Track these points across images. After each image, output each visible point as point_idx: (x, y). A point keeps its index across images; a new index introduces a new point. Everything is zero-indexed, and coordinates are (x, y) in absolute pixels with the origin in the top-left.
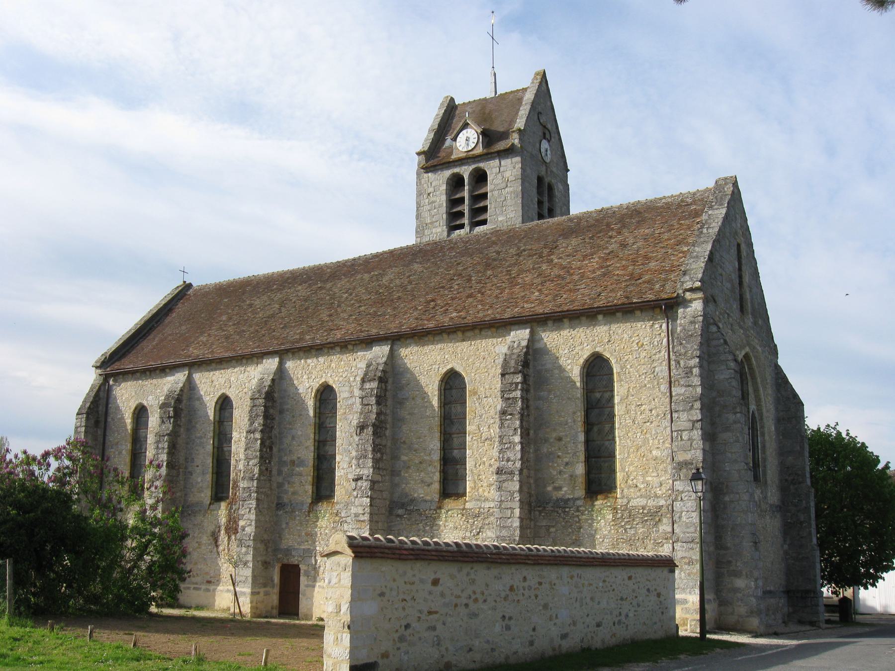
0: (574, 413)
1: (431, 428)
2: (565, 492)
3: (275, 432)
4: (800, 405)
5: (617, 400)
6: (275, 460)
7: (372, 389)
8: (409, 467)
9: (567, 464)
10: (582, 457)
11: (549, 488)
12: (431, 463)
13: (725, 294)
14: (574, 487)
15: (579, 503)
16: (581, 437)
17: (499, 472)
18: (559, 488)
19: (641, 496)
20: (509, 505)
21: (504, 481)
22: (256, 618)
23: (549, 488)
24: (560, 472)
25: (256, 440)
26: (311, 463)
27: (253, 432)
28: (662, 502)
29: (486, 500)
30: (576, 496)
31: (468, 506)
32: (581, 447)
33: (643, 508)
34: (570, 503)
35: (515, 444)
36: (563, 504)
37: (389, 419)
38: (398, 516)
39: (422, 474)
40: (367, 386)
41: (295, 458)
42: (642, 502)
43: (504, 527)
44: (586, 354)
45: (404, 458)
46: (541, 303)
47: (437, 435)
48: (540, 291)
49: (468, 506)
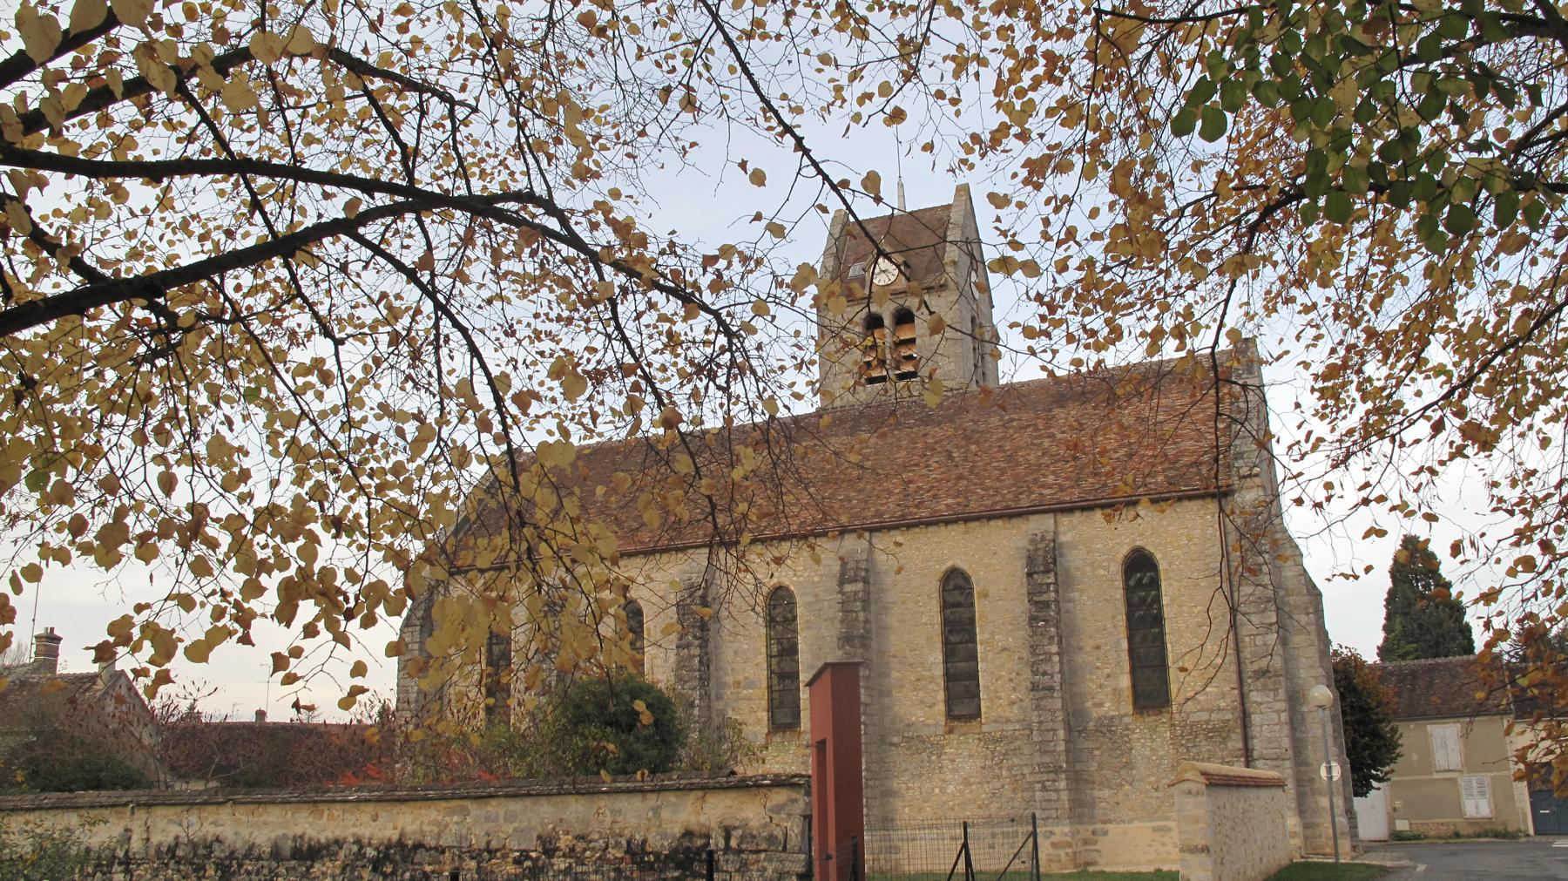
0: (1114, 617)
1: (929, 639)
2: (1108, 708)
3: (711, 645)
4: (1320, 595)
5: (1165, 600)
6: (712, 682)
7: (856, 593)
8: (902, 686)
9: (1108, 676)
10: (1127, 668)
11: (1088, 704)
12: (932, 679)
13: (482, 331)
14: (1119, 702)
15: (1127, 720)
16: (1125, 645)
17: (1035, 687)
18: (1101, 705)
19: (1202, 710)
20: (1050, 726)
21: (1042, 699)
22: (1403, 868)
23: (1088, 704)
24: (1101, 686)
25: (692, 657)
26: (764, 684)
27: (688, 646)
28: (1229, 716)
29: (1008, 721)
30: (1123, 711)
31: (985, 728)
32: (1125, 657)
33: (1207, 722)
34: (1117, 721)
35: (1050, 654)
36: (1107, 726)
37: (873, 627)
38: (893, 744)
39: (921, 694)
40: (848, 588)
41: (740, 678)
42: (1204, 716)
43: (1045, 752)
44: (1125, 550)
45: (895, 674)
46: (1062, 489)
47: (939, 646)
48: (1054, 473)
49: (985, 728)
